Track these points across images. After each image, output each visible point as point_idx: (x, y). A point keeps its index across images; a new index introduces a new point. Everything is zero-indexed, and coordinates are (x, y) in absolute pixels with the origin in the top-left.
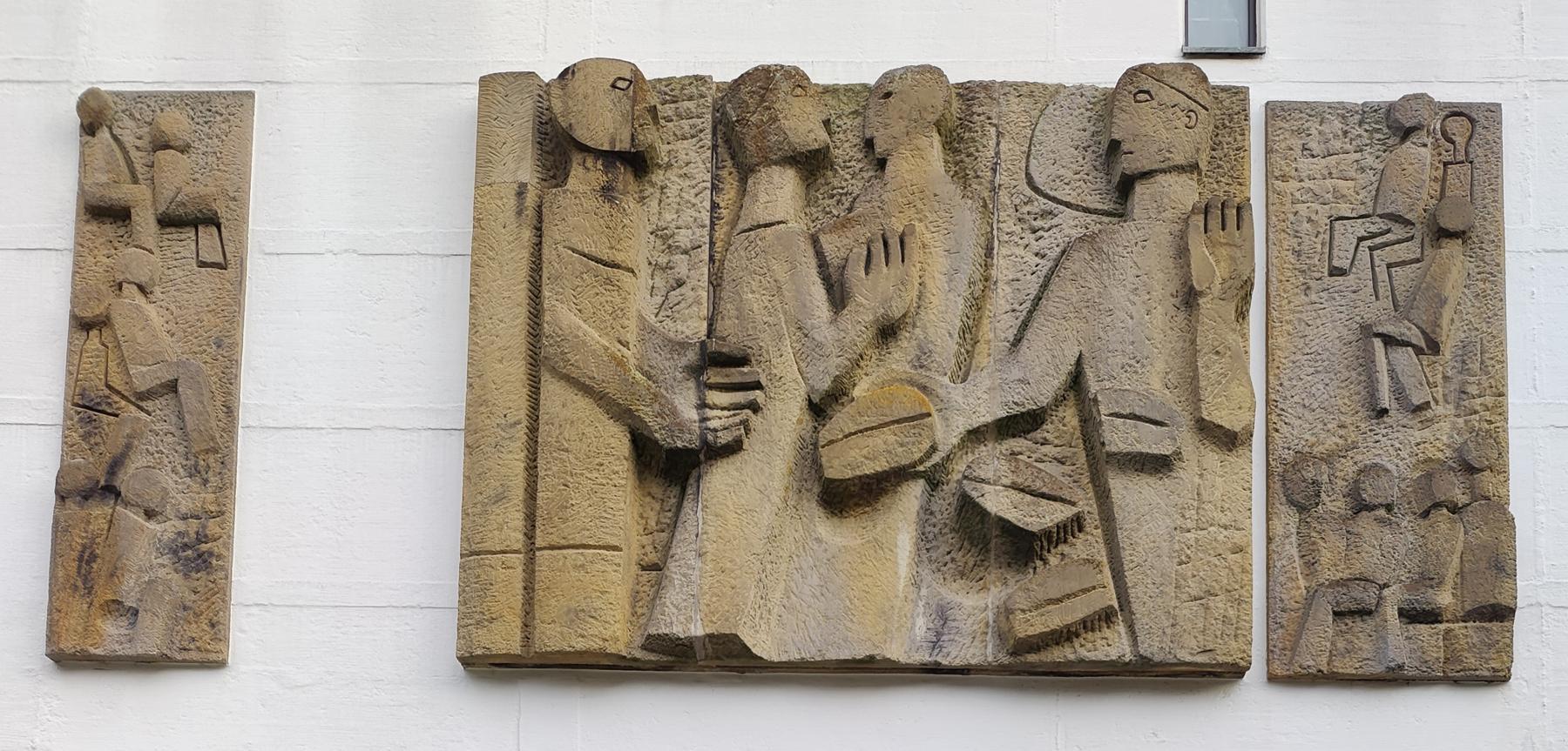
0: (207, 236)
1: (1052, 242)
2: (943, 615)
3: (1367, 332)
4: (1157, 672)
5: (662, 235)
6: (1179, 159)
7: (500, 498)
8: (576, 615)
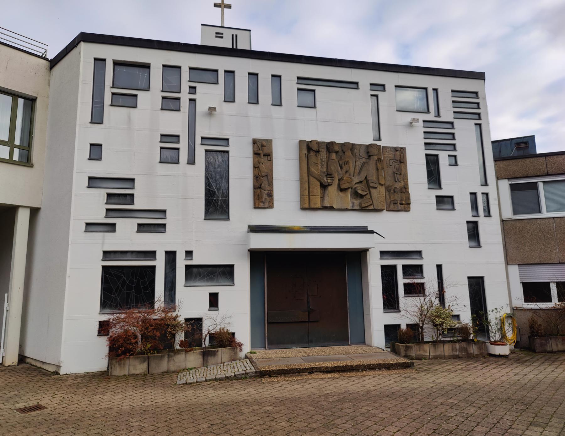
0: (269, 157)
1: (362, 161)
2: (353, 203)
3: (394, 172)
4: (226, 176)
5: (321, 160)
6: (375, 154)
7: (305, 190)
8: (315, 204)
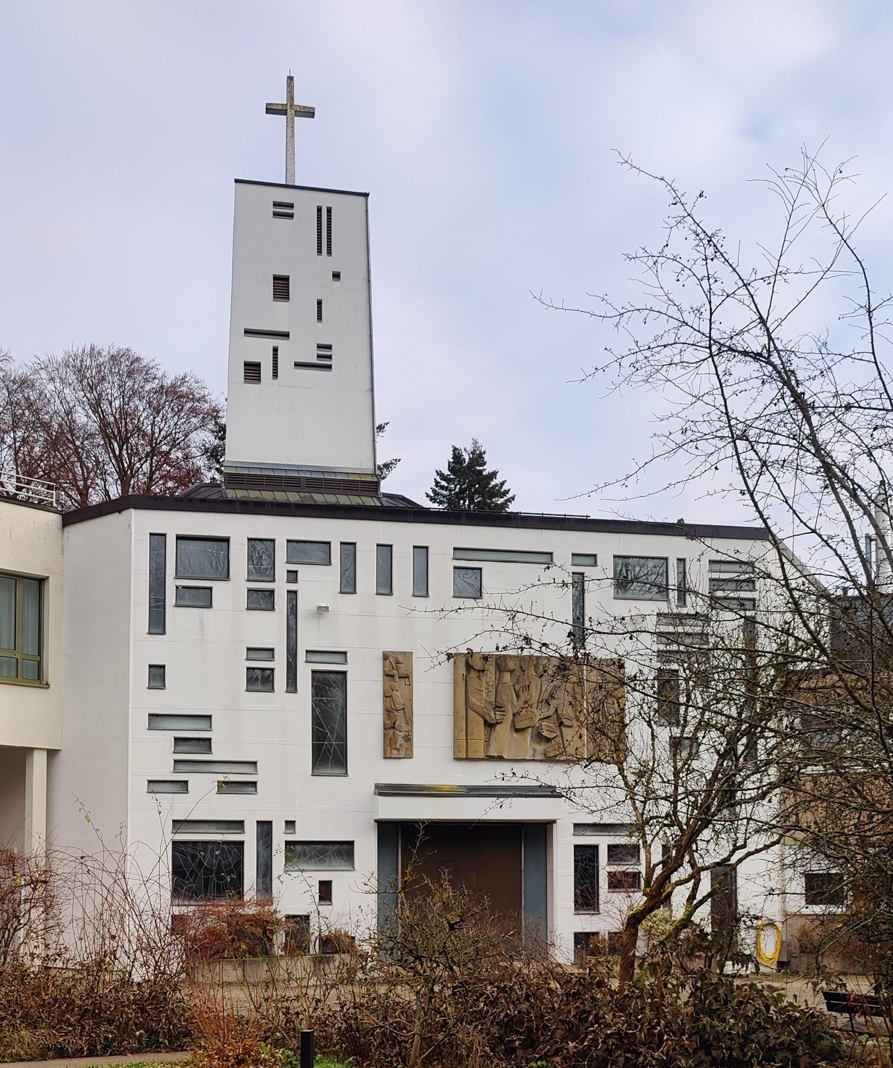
8: (476, 752)
